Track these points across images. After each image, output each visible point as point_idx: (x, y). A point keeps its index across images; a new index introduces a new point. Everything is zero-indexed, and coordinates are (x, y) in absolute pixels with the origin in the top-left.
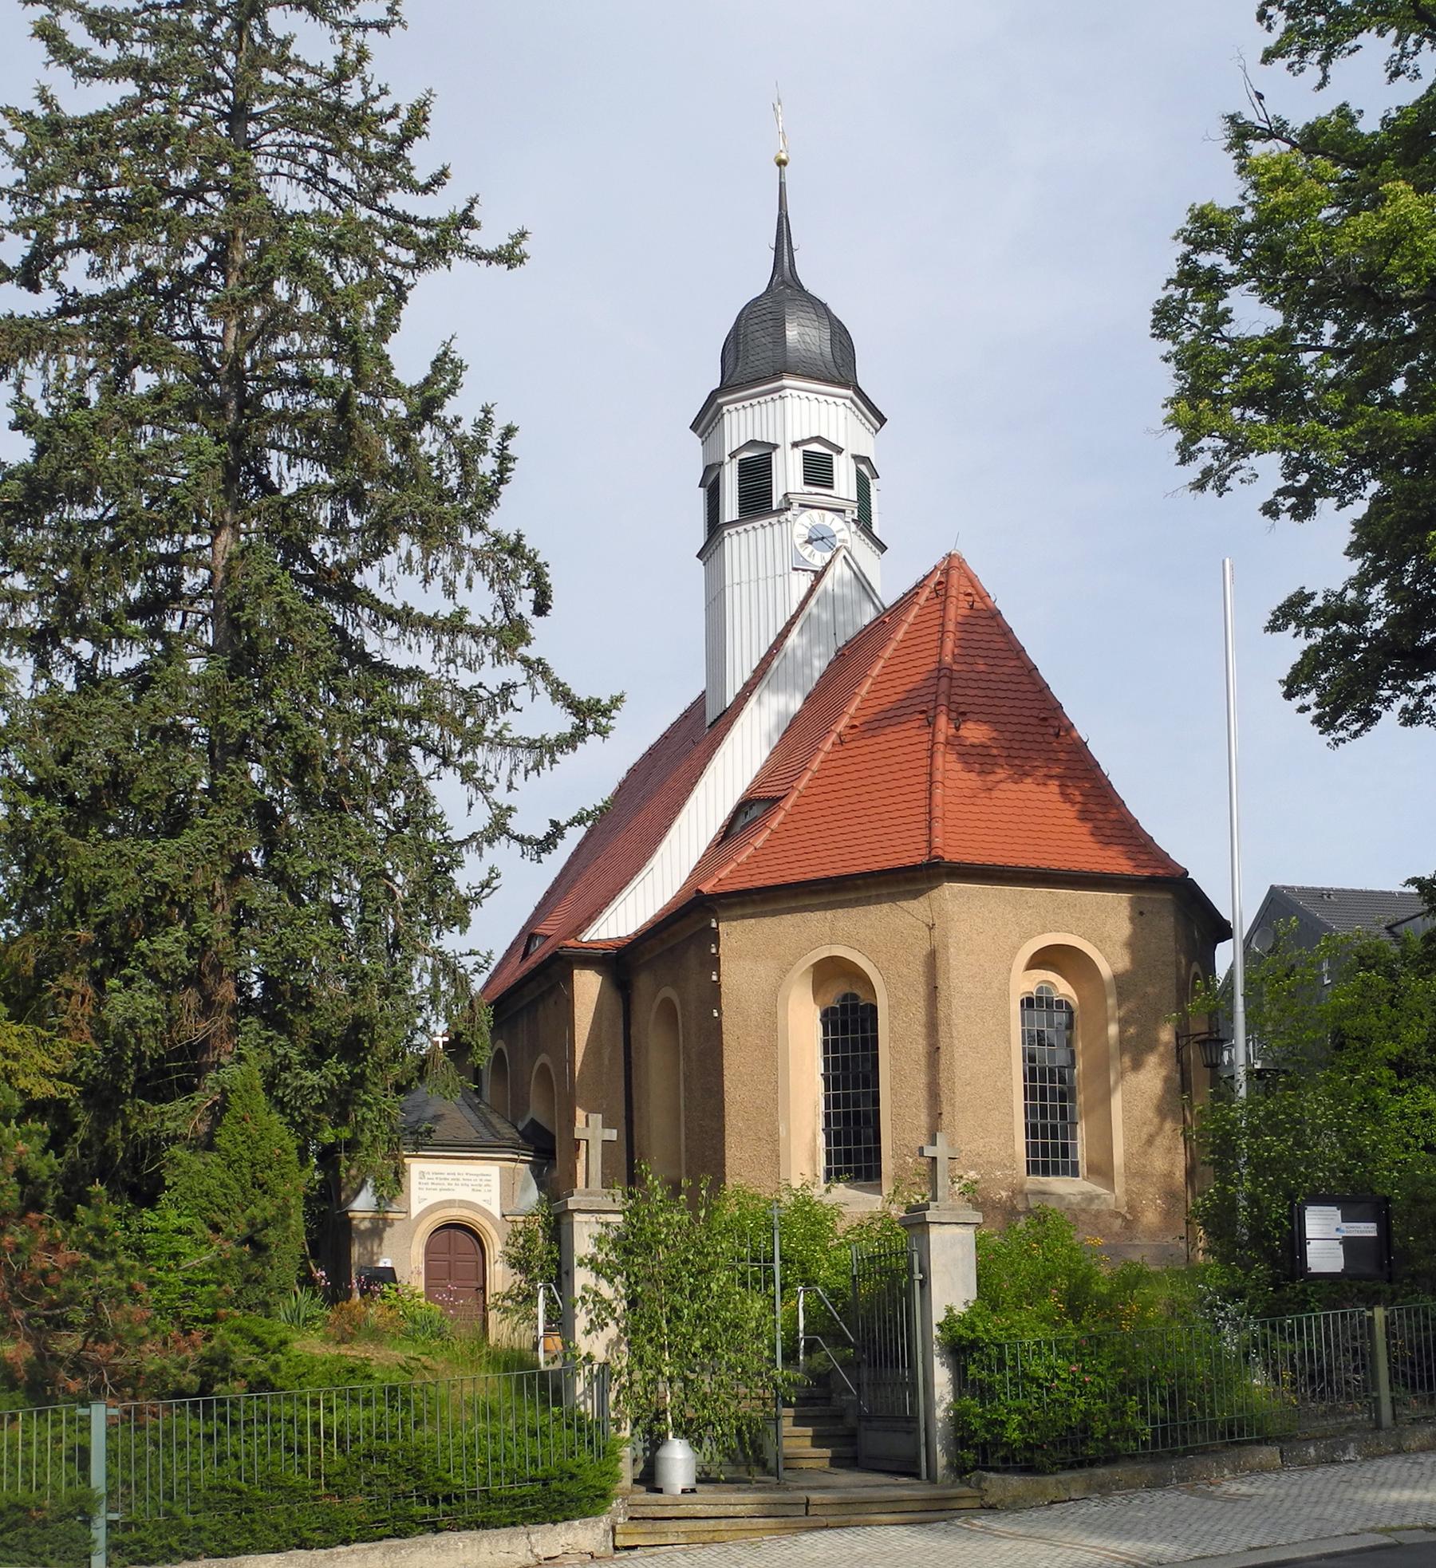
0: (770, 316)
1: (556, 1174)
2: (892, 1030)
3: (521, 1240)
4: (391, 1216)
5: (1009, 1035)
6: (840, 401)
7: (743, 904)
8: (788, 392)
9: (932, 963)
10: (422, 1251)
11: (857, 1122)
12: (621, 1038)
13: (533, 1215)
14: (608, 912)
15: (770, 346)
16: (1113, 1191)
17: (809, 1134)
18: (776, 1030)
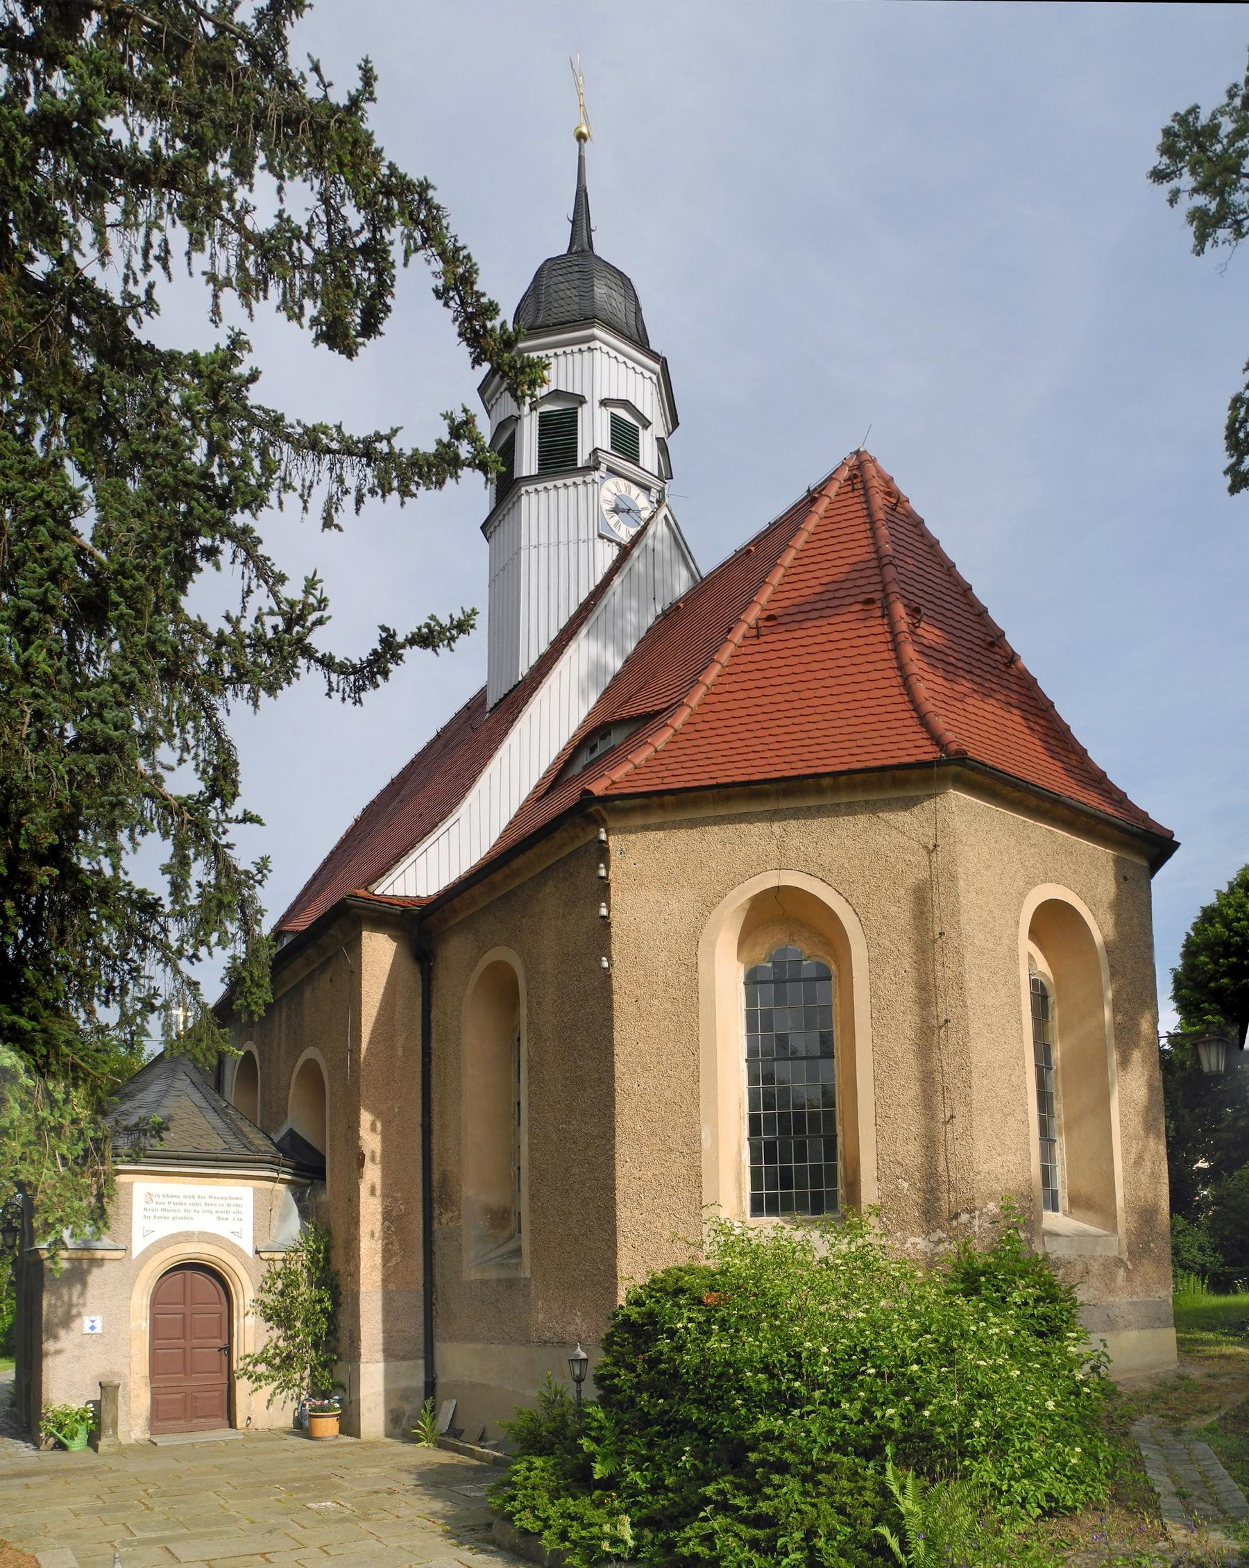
0: (576, 269)
1: (325, 1197)
2: (874, 994)
3: (279, 1285)
4: (99, 1254)
5: (1020, 1012)
6: (648, 374)
7: (645, 809)
8: (597, 344)
9: (922, 899)
10: (146, 1301)
11: (800, 1129)
12: (419, 1023)
13: (296, 1251)
14: (407, 861)
15: (577, 299)
16: (1115, 1230)
17: (735, 1147)
18: (696, 990)
